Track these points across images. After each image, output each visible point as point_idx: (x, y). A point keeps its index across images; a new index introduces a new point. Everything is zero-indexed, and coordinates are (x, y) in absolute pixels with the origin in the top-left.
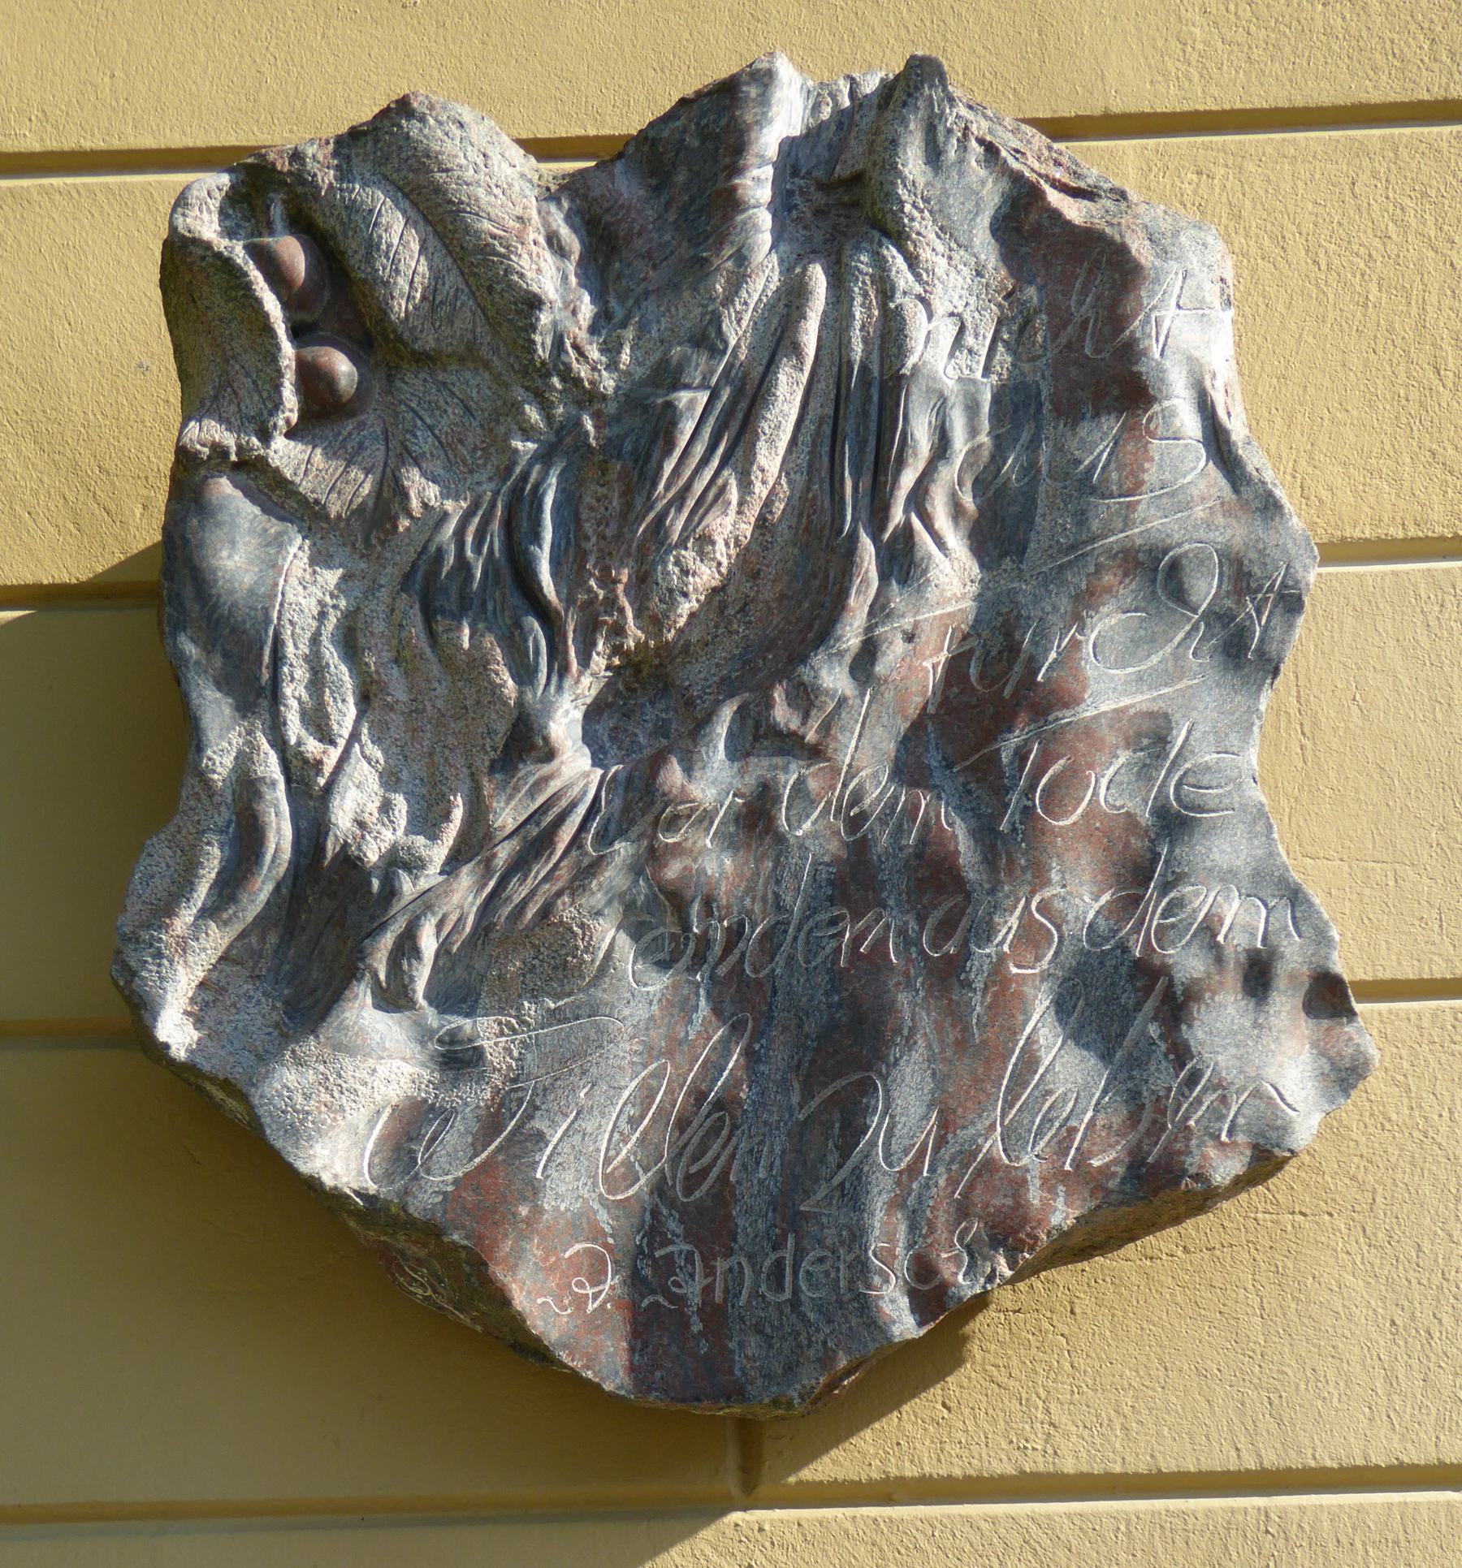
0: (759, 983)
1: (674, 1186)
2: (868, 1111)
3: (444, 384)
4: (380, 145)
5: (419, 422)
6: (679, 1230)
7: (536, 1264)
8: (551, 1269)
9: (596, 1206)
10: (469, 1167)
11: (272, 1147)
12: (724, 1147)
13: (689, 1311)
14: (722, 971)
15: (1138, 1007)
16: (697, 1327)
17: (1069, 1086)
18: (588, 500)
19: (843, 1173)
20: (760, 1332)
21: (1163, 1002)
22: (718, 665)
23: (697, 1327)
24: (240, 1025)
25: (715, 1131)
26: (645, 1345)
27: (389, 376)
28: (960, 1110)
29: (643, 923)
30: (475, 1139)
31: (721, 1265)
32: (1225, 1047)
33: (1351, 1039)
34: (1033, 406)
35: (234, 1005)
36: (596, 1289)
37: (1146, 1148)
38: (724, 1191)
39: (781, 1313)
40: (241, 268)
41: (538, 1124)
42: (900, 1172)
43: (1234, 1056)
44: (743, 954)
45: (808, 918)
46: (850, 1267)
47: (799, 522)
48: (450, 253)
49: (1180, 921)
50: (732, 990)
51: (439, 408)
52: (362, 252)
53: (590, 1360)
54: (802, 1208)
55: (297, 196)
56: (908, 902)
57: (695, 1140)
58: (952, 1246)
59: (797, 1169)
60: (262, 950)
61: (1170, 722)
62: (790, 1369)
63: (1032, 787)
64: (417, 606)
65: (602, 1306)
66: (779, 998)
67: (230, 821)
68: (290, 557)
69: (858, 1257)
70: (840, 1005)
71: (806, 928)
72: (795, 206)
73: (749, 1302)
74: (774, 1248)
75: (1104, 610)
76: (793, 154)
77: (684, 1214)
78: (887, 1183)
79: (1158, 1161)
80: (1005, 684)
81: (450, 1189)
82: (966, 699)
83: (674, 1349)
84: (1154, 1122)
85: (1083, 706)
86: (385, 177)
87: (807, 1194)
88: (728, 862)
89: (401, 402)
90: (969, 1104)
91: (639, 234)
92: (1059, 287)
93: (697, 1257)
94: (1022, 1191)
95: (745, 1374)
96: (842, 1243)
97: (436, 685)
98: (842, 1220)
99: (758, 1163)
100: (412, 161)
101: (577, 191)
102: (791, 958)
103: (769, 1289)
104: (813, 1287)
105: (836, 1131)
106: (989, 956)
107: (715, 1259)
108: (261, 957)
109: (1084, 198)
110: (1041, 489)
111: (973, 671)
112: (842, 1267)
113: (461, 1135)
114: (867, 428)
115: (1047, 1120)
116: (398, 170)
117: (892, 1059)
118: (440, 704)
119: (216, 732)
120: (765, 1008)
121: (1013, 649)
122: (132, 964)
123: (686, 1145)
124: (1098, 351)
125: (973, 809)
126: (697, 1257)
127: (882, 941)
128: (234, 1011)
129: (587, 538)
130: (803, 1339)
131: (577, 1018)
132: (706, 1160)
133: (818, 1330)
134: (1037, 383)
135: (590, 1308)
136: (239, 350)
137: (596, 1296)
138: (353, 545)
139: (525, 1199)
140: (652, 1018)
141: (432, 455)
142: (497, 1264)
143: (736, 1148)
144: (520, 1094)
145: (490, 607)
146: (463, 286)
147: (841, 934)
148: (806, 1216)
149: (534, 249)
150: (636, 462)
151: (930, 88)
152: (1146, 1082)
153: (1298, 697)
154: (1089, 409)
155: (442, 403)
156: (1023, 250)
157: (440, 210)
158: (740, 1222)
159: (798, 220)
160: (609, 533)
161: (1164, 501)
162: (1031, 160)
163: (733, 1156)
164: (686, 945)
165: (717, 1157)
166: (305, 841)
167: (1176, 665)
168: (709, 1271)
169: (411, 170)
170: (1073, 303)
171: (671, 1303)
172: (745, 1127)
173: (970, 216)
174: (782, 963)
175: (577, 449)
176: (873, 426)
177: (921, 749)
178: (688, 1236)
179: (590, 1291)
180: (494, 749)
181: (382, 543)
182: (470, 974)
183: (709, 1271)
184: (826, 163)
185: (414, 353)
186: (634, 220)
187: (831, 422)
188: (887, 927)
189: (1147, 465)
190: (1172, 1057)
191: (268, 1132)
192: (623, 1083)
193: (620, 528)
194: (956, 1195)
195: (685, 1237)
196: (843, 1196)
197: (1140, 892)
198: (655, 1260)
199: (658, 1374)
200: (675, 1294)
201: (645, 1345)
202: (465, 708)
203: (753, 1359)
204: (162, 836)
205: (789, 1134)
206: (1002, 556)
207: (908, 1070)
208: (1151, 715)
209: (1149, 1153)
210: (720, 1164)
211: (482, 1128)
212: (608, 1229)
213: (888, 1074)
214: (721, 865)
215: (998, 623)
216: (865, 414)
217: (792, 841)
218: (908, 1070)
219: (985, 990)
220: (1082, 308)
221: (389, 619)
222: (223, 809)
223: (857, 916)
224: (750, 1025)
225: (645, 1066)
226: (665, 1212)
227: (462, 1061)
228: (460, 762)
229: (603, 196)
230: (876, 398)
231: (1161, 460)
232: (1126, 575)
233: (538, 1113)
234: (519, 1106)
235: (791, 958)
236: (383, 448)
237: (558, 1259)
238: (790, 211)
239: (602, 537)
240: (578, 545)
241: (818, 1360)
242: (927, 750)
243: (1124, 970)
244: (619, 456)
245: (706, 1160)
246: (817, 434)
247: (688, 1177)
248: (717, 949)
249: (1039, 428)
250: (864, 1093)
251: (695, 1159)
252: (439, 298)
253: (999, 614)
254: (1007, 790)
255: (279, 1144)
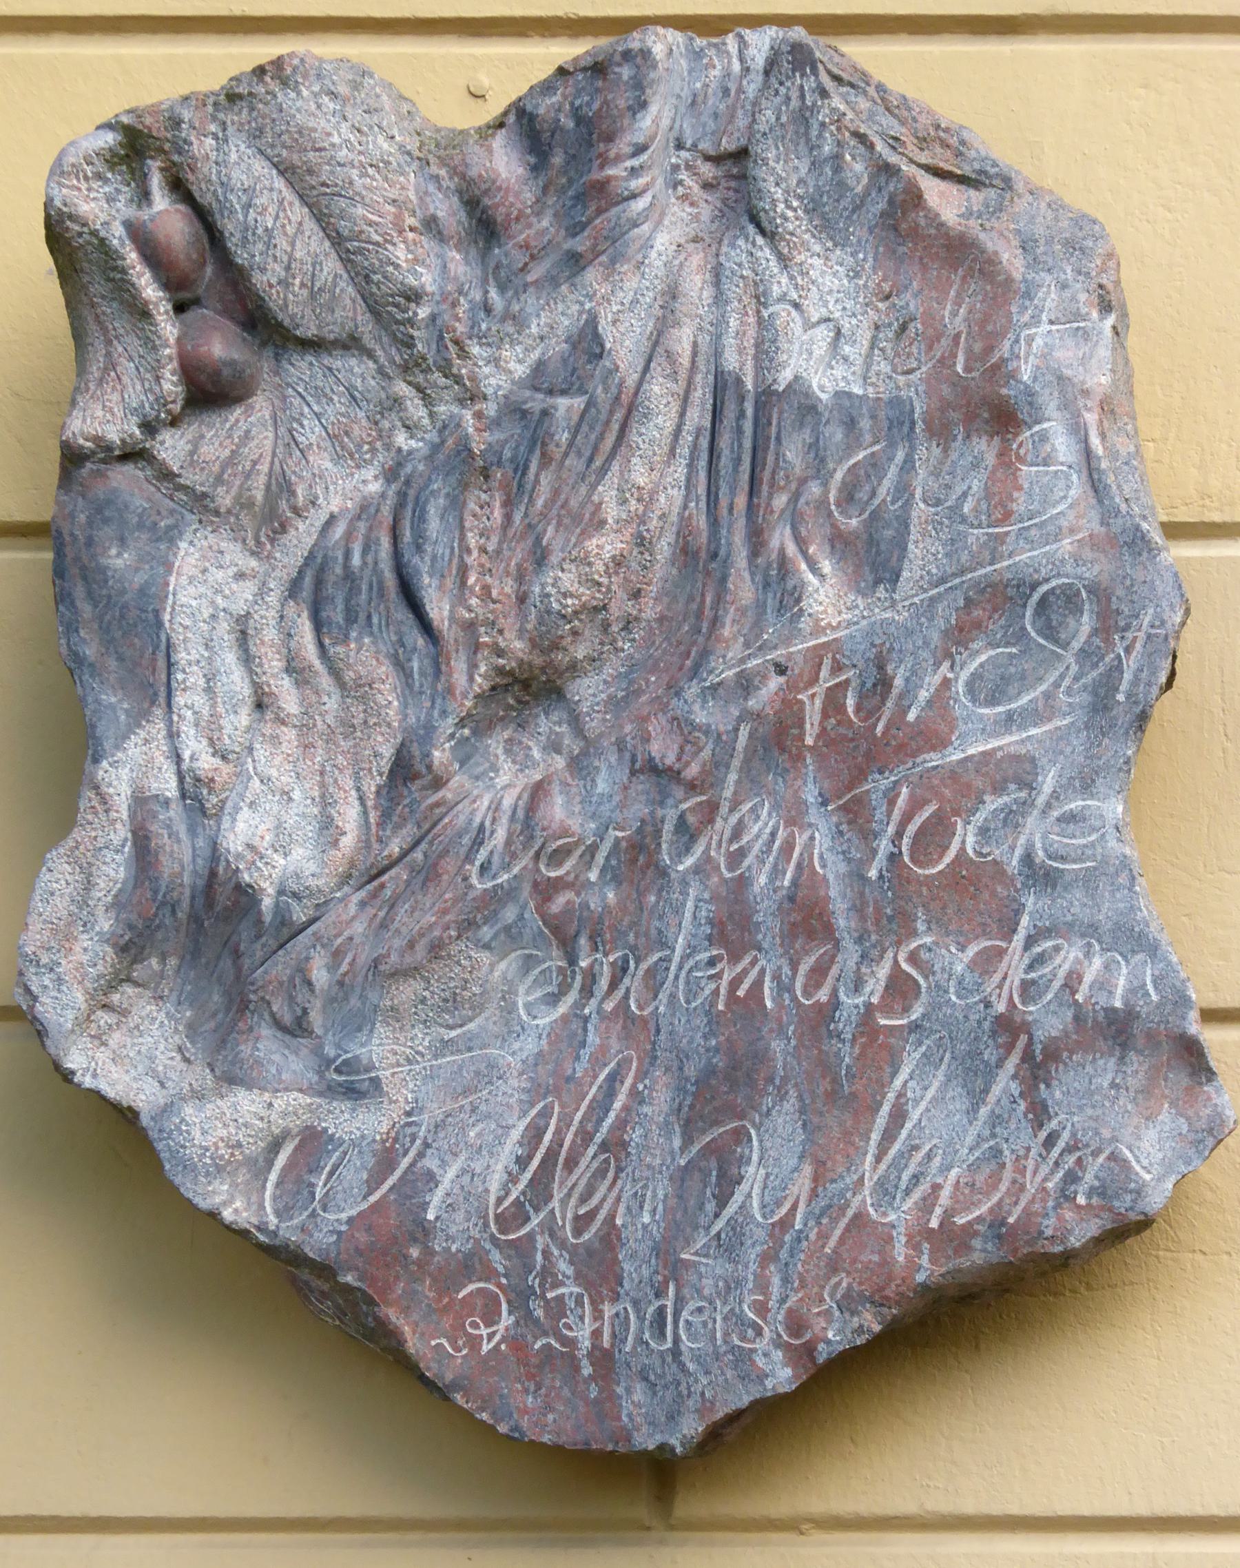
0: (644, 1021)
1: (564, 1226)
2: (744, 1161)
3: (330, 369)
4: (255, 114)
5: (306, 410)
6: (570, 1271)
7: (429, 1306)
8: (445, 1310)
9: (488, 1246)
10: (364, 1206)
11: (171, 1182)
12: (610, 1189)
13: (579, 1354)
14: (609, 1006)
15: (1000, 1064)
16: (587, 1370)
17: (935, 1141)
18: (472, 505)
19: (720, 1224)
20: (646, 1379)
21: (1023, 1060)
22: (605, 682)
23: (587, 1370)
24: (143, 1049)
25: (601, 1173)
26: (538, 1387)
27: (277, 354)
28: (829, 1164)
29: (530, 956)
30: (370, 1176)
31: (608, 1310)
32: (1081, 1108)
33: (1209, 1099)
34: (907, 424)
35: (137, 1027)
36: (490, 1330)
37: (1006, 1208)
38: (611, 1237)
39: (664, 1361)
40: (116, 251)
41: (430, 1163)
42: (773, 1225)
43: (1091, 1118)
44: (628, 990)
45: (689, 956)
46: (725, 1319)
47: (677, 541)
48: (328, 236)
49: (1041, 977)
50: (619, 1026)
51: (326, 395)
52: (238, 235)
53: (484, 1401)
54: (683, 1256)
55: (174, 164)
56: (782, 945)
57: (583, 1182)
58: (822, 1300)
59: (679, 1216)
60: (162, 971)
61: (1036, 767)
62: (672, 1417)
63: (899, 834)
64: (305, 614)
65: (496, 1348)
66: (662, 1037)
67: (126, 840)
68: (182, 553)
69: (732, 1310)
70: (717, 1050)
71: (687, 967)
72: (681, 182)
73: (634, 1348)
74: (658, 1295)
75: (975, 646)
76: (677, 126)
77: (573, 1251)
78: (760, 1234)
79: (1018, 1220)
80: (878, 719)
81: (344, 1228)
82: (842, 730)
83: (566, 1392)
84: (1014, 1182)
85: (950, 749)
86: (261, 152)
87: (688, 1242)
88: (611, 895)
89: (288, 385)
90: (839, 1157)
91: (517, 219)
92: (934, 294)
93: (586, 1300)
94: (888, 1247)
95: (631, 1420)
96: (718, 1293)
97: (325, 699)
98: (719, 1271)
99: (641, 1207)
100: (285, 137)
101: (455, 168)
102: (673, 997)
103: (652, 1337)
104: (693, 1337)
105: (714, 1179)
106: (857, 1007)
107: (603, 1302)
108: (162, 978)
109: (969, 185)
110: (914, 514)
111: (850, 702)
112: (719, 1318)
113: (357, 1171)
114: (740, 446)
115: (916, 1179)
116: (273, 146)
117: (764, 1108)
118: (330, 720)
119: (112, 741)
120: (649, 1047)
121: (884, 684)
122: (33, 988)
123: (574, 1185)
124: (968, 369)
125: (843, 852)
126: (586, 1300)
127: (758, 984)
128: (136, 1033)
129: (469, 551)
130: (683, 1388)
131: (470, 1049)
132: (594, 1201)
133: (696, 1381)
134: (911, 399)
135: (486, 1347)
136: (122, 331)
137: (491, 1336)
138: (244, 541)
139: (415, 1240)
140: (540, 1054)
141: (319, 447)
142: (389, 1304)
143: (621, 1191)
144: (413, 1129)
145: (375, 620)
146: (341, 272)
147: (718, 976)
148: (687, 1264)
149: (411, 235)
150: (515, 471)
151: (802, 76)
152: (1007, 1140)
153: (1223, 694)
154: (960, 431)
155: (328, 390)
156: (902, 249)
157: (315, 192)
158: (626, 1266)
159: (684, 198)
160: (491, 548)
161: (1033, 532)
162: (910, 147)
163: (618, 1199)
164: (573, 978)
165: (603, 1200)
166: (200, 861)
167: (1045, 705)
168: (598, 1315)
169: (284, 146)
170: (947, 314)
171: (563, 1345)
172: (629, 1169)
173: (846, 214)
174: (665, 1001)
175: (459, 453)
176: (747, 444)
177: (799, 782)
178: (579, 1277)
179: (484, 1332)
180: (381, 775)
181: (272, 541)
182: (364, 1004)
183: (598, 1315)
184: (713, 133)
185: (297, 338)
186: (512, 205)
187: (708, 434)
188: (762, 972)
189: (1016, 495)
190: (1031, 1116)
191: (167, 1167)
192: (510, 1122)
193: (500, 543)
194: (828, 1250)
195: (576, 1279)
196: (720, 1246)
197: (1004, 945)
198: (547, 1302)
199: (550, 1417)
200: (566, 1337)
201: (538, 1387)
202: (353, 726)
203: (638, 1405)
204: (62, 851)
205: (671, 1179)
206: (877, 582)
207: (780, 1121)
208: (1017, 758)
209: (1010, 1213)
210: (607, 1207)
211: (378, 1163)
212: (501, 1269)
213: (761, 1124)
214: (604, 898)
215: (871, 654)
216: (739, 431)
217: (673, 875)
218: (780, 1121)
219: (854, 1039)
220: (955, 318)
221: (280, 628)
222: (119, 826)
223: (735, 958)
224: (634, 1065)
225: (533, 1105)
226: (556, 1252)
227: (359, 1092)
228: (348, 783)
229: (480, 176)
230: (750, 412)
231: (1031, 488)
232: (995, 610)
233: (429, 1152)
234: (413, 1141)
235: (673, 997)
236: (271, 435)
237: (452, 1300)
238: (675, 187)
239: (483, 550)
240: (461, 557)
241: (697, 1411)
242: (805, 783)
243: (987, 1025)
244: (499, 463)
245: (594, 1201)
246: (695, 447)
247: (577, 1218)
248: (604, 983)
249: (913, 448)
250: (738, 1142)
251: (583, 1200)
252: (318, 285)
253: (873, 645)
254: (876, 836)
255: (178, 1180)
